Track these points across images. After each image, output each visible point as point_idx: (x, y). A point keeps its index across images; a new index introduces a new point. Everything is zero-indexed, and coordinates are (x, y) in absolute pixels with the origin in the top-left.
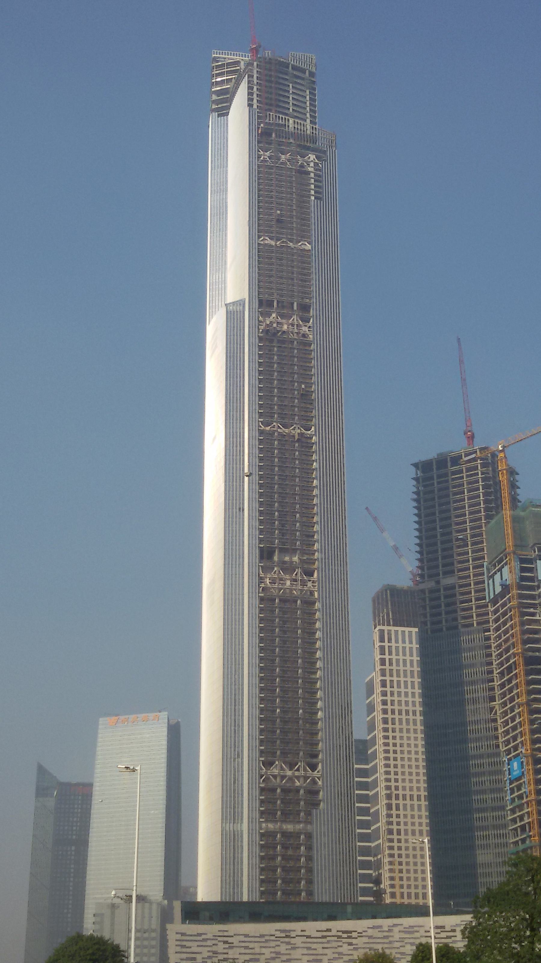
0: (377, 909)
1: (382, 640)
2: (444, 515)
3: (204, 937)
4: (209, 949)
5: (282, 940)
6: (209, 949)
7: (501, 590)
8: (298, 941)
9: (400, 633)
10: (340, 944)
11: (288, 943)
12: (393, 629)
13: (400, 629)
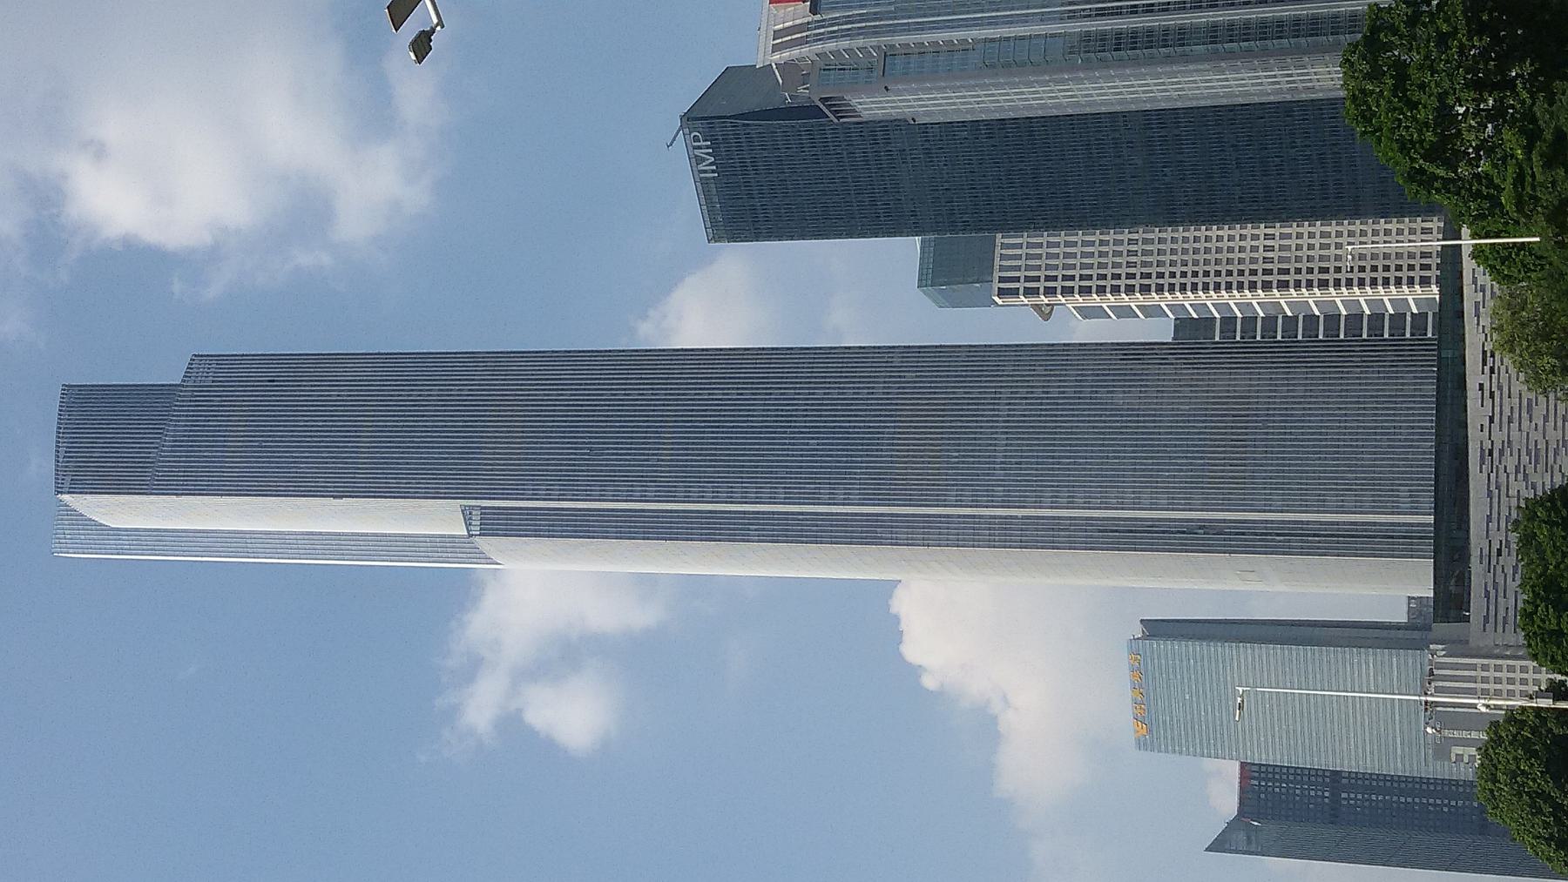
0: (1451, 312)
1: (1015, 292)
3: (1490, 588)
4: (1512, 477)
5: (1496, 463)
6: (1512, 477)
7: (913, 651)
9: (1002, 285)
11: (1501, 452)
12: (996, 275)
13: (997, 262)
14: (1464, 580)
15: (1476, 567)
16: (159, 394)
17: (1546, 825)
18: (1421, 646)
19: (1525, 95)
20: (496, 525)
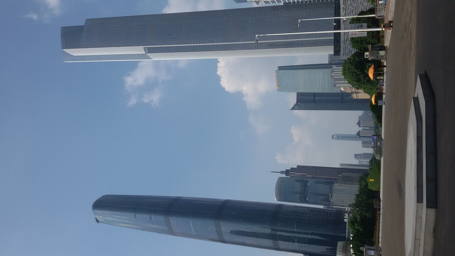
14: (340, 47)
15: (342, 44)
16: (82, 27)
17: (355, 78)
18: (331, 68)
19: (362, 95)
20: (151, 51)
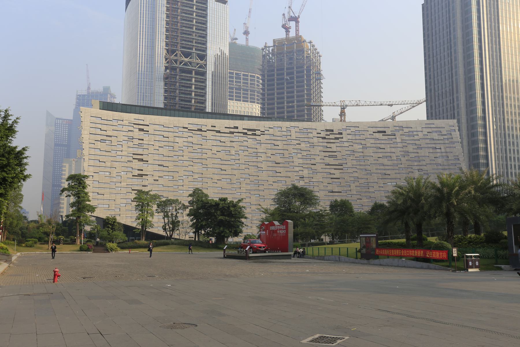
2: (289, 71)
8: (209, 134)
10: (246, 139)
